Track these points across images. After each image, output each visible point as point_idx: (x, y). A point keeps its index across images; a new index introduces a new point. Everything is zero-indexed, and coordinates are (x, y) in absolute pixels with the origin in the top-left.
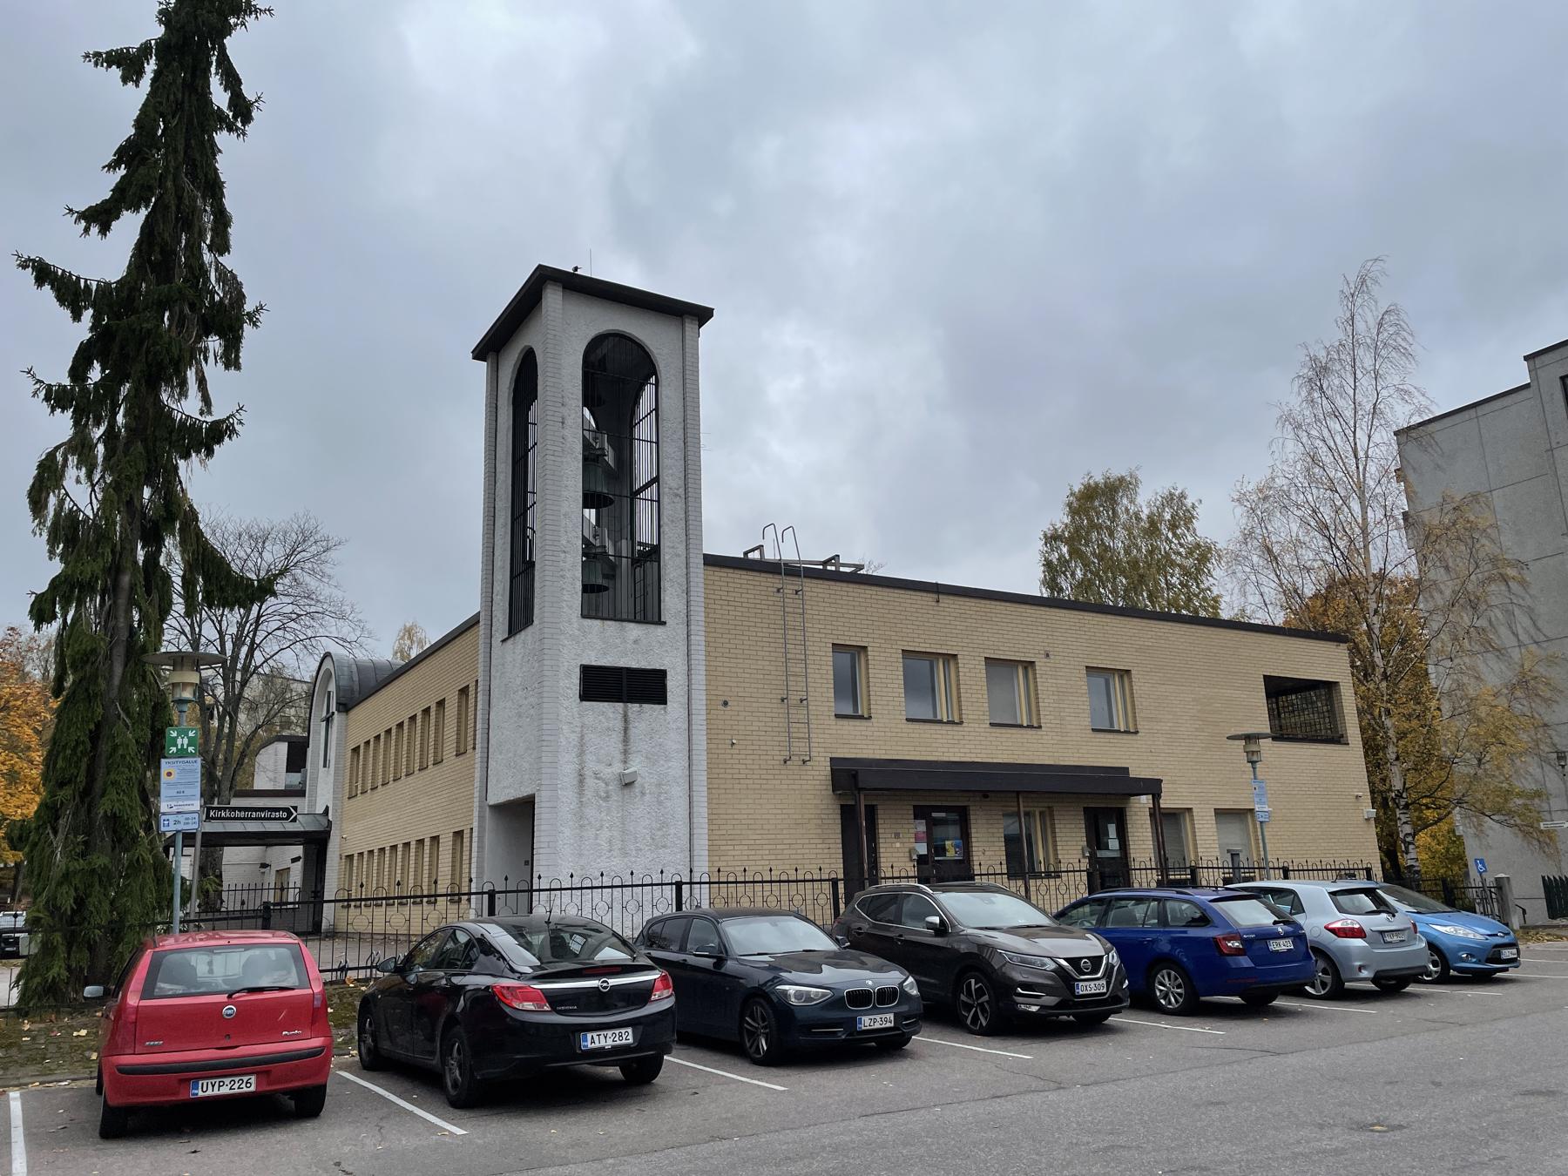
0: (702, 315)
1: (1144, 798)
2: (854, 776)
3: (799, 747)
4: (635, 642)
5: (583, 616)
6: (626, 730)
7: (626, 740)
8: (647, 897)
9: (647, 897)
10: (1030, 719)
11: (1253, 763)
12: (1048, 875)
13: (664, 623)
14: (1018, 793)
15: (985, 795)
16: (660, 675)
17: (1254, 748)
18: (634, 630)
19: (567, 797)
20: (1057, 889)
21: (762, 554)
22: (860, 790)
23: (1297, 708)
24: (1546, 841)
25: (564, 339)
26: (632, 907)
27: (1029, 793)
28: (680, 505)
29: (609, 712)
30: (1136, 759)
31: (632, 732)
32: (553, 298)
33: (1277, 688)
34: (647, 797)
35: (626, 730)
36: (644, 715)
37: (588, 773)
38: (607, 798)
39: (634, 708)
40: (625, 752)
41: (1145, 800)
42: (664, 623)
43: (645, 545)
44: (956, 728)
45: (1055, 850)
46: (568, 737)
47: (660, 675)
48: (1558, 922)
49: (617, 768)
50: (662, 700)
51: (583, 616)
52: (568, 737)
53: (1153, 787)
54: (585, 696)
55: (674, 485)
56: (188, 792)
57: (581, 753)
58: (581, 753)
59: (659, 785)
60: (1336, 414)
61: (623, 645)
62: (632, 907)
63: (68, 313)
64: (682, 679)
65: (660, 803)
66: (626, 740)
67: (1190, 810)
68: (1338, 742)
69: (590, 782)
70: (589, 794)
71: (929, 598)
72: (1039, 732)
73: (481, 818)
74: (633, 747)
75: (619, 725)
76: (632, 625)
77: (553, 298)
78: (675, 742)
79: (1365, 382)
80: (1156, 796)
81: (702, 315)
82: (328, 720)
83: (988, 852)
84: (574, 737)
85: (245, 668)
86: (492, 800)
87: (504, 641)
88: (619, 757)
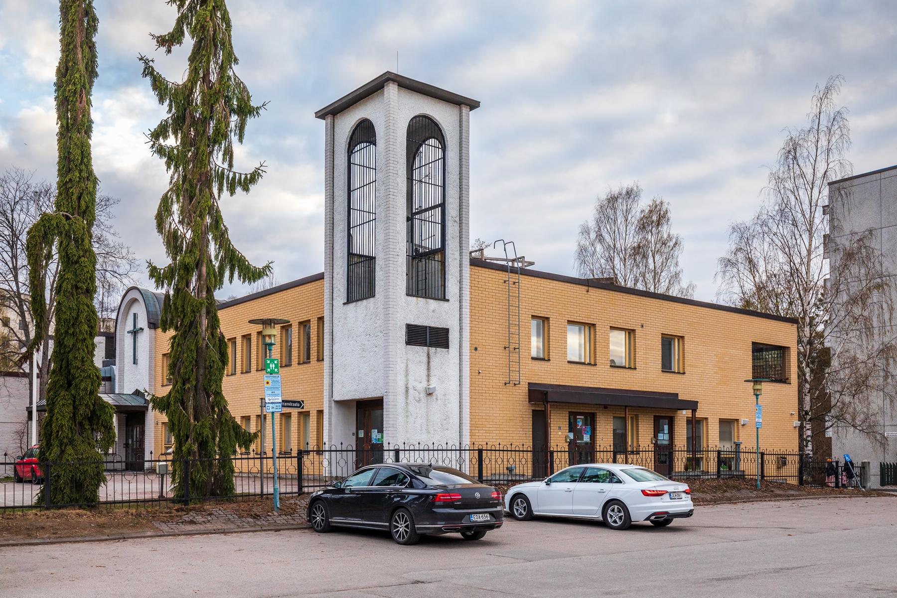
0: (473, 105)
1: (684, 412)
2: (545, 394)
3: (515, 377)
4: (433, 311)
5: (408, 295)
6: (429, 362)
7: (428, 369)
8: (440, 456)
9: (440, 456)
10: (630, 363)
11: (757, 395)
12: (632, 452)
13: (448, 300)
14: (626, 407)
15: (605, 407)
16: (446, 331)
17: (758, 387)
18: (433, 304)
19: (401, 399)
20: (451, 461)
21: (482, 254)
22: (547, 402)
23: (767, 364)
24: (883, 442)
25: (394, 114)
26: (499, 461)
27: (627, 405)
28: (457, 228)
29: (420, 352)
30: (679, 386)
31: (432, 364)
32: (392, 90)
33: (758, 349)
34: (439, 401)
35: (429, 362)
36: (438, 354)
37: (410, 386)
38: (419, 401)
39: (432, 350)
40: (428, 376)
41: (686, 413)
42: (448, 300)
43: (425, 248)
44: (593, 368)
45: (638, 439)
46: (400, 367)
47: (446, 331)
48: (885, 488)
49: (425, 384)
50: (446, 346)
51: (408, 295)
52: (400, 367)
53: (693, 406)
54: (409, 342)
55: (454, 215)
56: (276, 392)
57: (407, 375)
58: (407, 375)
59: (445, 395)
60: (803, 175)
61: (426, 313)
62: (499, 461)
63: (157, 99)
64: (457, 334)
65: (445, 405)
66: (428, 369)
67: (706, 419)
68: (785, 382)
69: (411, 391)
70: (410, 397)
71: (582, 289)
72: (684, 376)
73: (330, 407)
74: (432, 373)
75: (425, 359)
76: (432, 301)
77: (392, 90)
78: (453, 371)
79: (821, 158)
80: (694, 411)
81: (473, 105)
82: (135, 333)
83: (605, 437)
84: (403, 366)
85: (186, 313)
86: (337, 397)
87: (344, 304)
88: (425, 378)
